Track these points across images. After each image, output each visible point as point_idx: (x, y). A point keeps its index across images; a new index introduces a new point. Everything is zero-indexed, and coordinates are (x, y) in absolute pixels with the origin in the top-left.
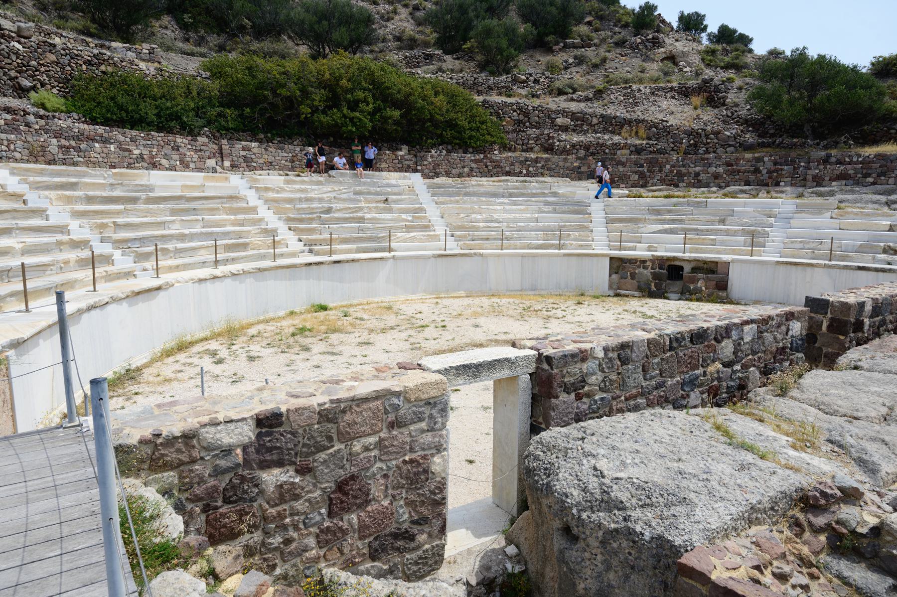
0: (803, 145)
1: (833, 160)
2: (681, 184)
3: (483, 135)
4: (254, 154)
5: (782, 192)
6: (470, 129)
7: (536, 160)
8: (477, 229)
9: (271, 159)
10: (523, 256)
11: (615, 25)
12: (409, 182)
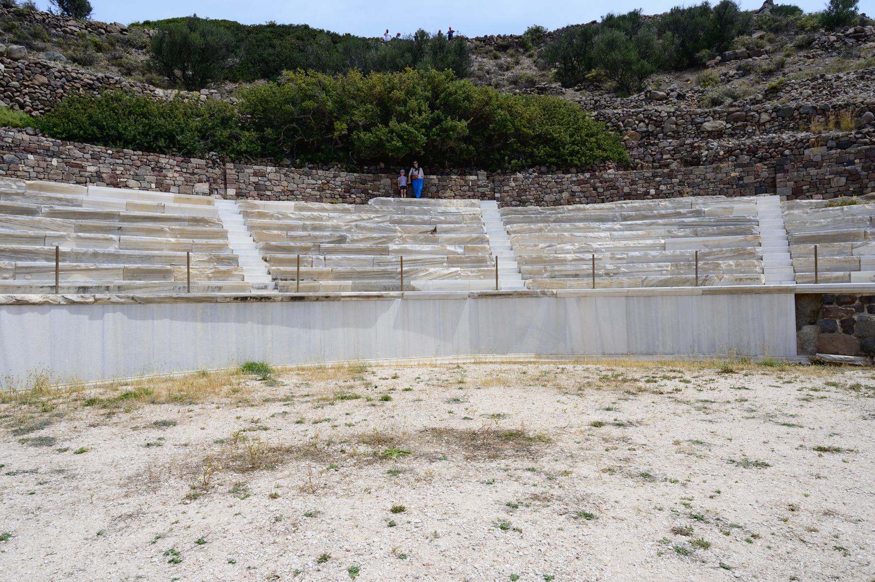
6: (573, 143)
8: (563, 262)
9: (292, 187)
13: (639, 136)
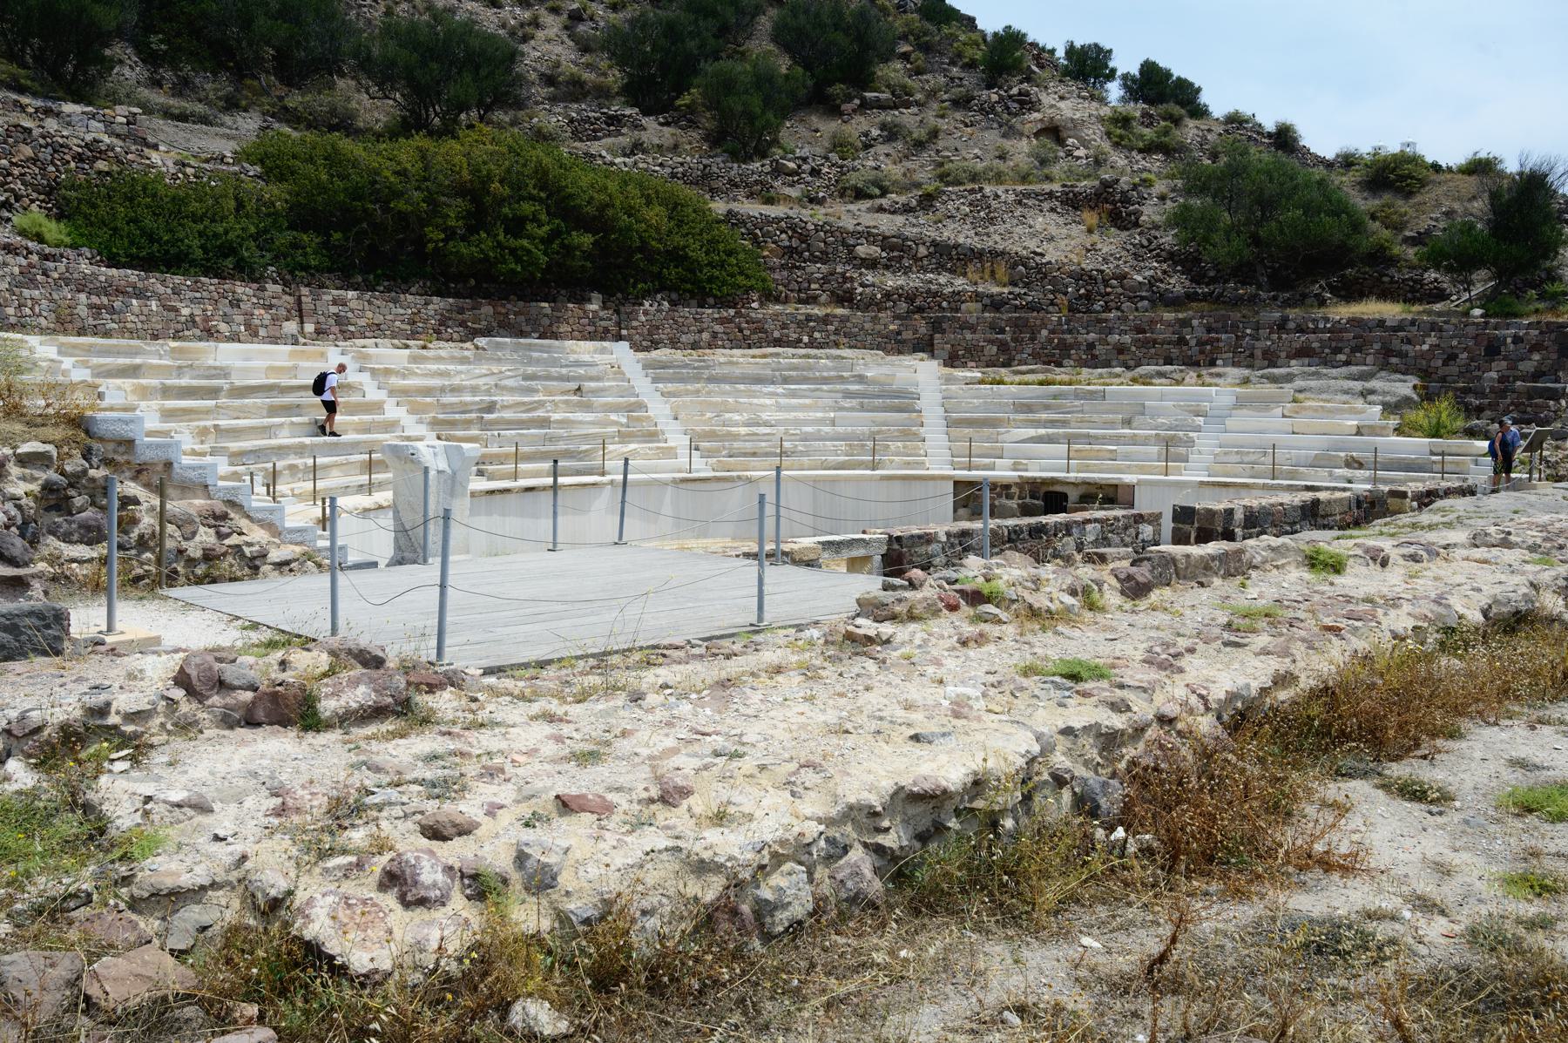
0: (1252, 300)
1: (1292, 325)
2: (1065, 362)
3: (732, 275)
4: (352, 311)
5: (1219, 375)
6: (710, 264)
7: (826, 320)
9: (379, 319)
10: (816, 480)
11: (953, 63)
12: (612, 358)
13: (780, 252)
